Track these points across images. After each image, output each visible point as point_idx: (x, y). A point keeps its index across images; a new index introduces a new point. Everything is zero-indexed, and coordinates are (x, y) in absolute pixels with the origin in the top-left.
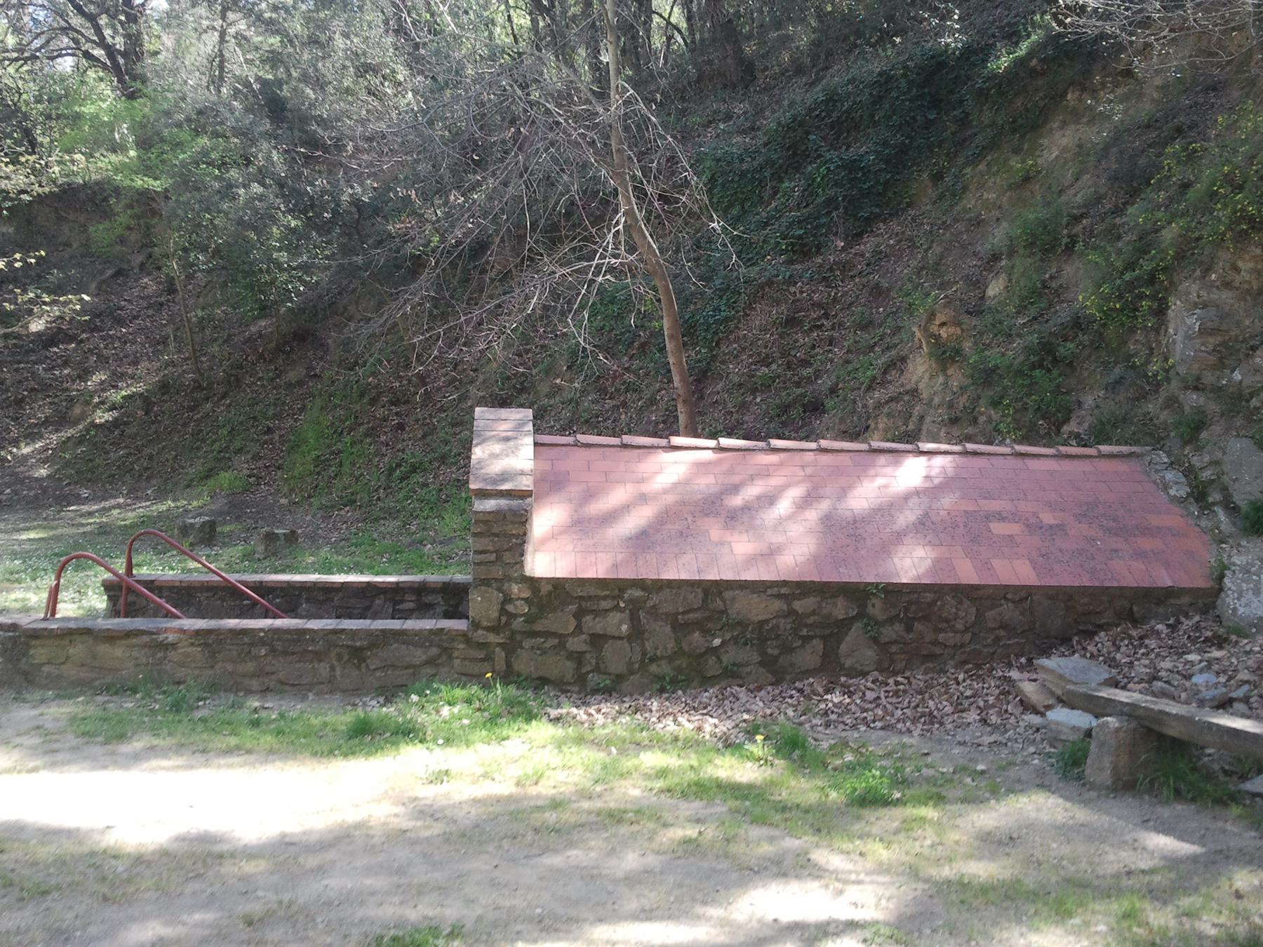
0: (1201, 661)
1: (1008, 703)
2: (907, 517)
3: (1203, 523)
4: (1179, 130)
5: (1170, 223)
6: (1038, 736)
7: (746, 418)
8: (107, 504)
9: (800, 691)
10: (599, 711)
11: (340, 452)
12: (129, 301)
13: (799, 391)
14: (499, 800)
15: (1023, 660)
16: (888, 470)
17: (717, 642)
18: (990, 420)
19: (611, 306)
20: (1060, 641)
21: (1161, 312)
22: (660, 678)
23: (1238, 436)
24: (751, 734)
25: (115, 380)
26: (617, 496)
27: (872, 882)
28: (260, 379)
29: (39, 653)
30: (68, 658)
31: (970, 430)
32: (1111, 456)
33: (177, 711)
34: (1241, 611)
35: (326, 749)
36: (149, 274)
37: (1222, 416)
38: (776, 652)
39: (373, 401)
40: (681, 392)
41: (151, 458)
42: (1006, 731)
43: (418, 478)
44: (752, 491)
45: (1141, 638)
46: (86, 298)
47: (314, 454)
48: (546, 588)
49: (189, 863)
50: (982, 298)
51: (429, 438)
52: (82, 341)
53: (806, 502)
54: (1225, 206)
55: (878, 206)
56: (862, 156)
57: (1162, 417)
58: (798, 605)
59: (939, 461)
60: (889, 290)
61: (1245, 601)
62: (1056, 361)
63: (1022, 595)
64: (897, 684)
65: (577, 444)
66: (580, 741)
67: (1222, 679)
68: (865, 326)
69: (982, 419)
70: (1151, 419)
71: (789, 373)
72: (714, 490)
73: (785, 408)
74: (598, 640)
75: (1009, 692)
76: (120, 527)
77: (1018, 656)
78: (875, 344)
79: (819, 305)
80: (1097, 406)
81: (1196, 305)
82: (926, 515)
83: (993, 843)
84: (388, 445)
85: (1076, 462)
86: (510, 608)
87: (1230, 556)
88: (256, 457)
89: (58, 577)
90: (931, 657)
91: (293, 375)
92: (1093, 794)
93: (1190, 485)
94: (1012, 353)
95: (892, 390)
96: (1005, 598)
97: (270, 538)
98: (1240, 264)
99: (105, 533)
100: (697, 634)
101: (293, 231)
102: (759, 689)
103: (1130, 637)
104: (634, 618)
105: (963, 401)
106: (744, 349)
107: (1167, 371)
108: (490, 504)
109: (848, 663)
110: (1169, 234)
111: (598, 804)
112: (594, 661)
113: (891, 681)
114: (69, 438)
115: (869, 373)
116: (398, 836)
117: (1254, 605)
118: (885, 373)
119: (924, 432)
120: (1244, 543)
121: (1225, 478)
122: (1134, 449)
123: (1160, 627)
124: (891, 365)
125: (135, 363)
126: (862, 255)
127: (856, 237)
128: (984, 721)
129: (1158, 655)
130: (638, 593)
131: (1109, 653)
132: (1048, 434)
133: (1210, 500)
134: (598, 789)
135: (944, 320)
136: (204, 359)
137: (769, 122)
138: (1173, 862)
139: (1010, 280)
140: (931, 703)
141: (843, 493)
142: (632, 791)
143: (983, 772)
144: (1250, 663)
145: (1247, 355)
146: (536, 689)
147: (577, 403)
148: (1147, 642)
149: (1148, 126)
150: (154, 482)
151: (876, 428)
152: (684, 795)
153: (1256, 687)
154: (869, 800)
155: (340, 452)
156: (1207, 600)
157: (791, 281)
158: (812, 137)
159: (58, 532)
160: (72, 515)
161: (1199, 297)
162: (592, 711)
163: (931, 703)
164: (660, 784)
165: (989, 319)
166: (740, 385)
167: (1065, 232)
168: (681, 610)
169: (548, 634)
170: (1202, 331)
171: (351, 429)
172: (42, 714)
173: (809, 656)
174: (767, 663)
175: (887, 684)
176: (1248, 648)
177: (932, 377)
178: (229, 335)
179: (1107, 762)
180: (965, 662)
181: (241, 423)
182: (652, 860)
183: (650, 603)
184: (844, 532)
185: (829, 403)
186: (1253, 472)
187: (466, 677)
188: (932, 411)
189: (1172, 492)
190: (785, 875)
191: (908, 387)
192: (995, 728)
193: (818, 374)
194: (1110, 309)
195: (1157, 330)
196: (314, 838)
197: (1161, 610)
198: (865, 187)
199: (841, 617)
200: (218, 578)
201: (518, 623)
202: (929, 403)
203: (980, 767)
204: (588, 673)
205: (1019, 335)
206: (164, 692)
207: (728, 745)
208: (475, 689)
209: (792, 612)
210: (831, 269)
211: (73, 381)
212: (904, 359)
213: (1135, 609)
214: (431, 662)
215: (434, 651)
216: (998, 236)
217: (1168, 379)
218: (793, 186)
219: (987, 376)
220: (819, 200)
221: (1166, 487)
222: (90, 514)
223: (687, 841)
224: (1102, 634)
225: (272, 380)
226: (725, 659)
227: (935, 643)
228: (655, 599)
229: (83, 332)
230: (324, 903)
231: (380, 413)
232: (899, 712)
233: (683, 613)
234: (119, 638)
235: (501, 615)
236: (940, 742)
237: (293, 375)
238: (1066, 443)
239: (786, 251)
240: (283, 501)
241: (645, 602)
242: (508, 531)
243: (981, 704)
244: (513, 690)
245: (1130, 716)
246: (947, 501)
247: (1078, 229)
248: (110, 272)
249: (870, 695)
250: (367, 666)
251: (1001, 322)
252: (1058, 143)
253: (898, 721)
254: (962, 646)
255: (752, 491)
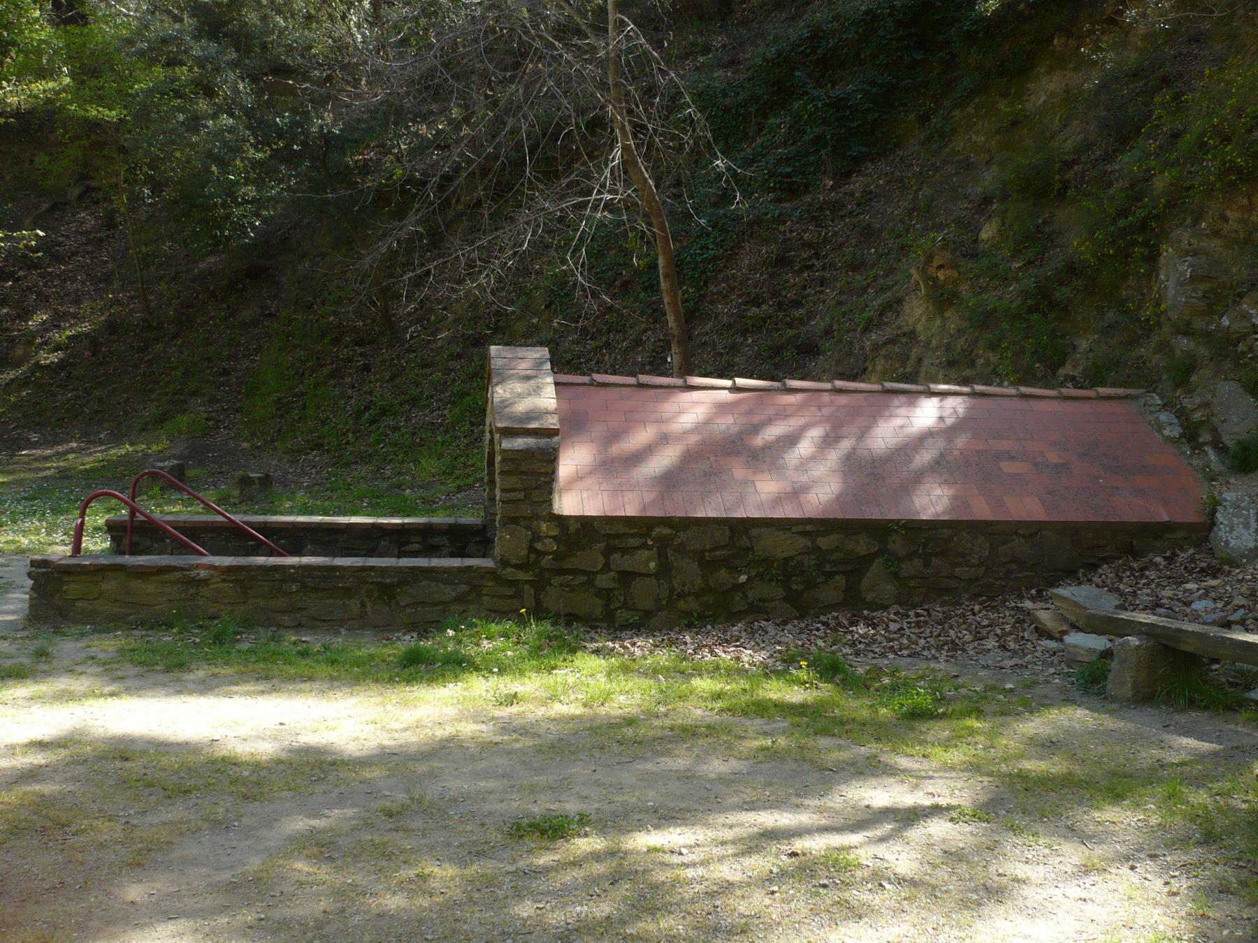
0: (1198, 589)
1: (1024, 630)
2: (925, 457)
3: (1195, 462)
4: (1166, 81)
5: (1162, 172)
6: (1055, 659)
7: (737, 360)
8: (60, 449)
9: (825, 624)
10: (634, 644)
11: (303, 394)
12: (67, 237)
13: (791, 332)
14: (573, 718)
15: (1033, 592)
16: (903, 411)
17: (743, 578)
18: (988, 363)
19: (607, 243)
20: (1070, 574)
21: (1152, 258)
22: (687, 614)
23: (1226, 379)
24: (790, 661)
25: (56, 323)
26: (641, 437)
27: (941, 778)
28: (212, 318)
29: (72, 588)
30: (101, 593)
31: (968, 373)
32: (1108, 398)
33: (221, 644)
34: (1233, 543)
35: (386, 677)
36: (86, 208)
37: (1212, 359)
38: (800, 587)
39: (336, 341)
40: (676, 332)
41: (101, 401)
42: (1025, 655)
43: (389, 421)
44: (774, 431)
45: (1142, 569)
46: (41, 234)
47: (276, 396)
48: (573, 527)
49: (307, 769)
50: (976, 241)
51: (397, 381)
52: (18, 279)
53: (828, 442)
54: (1215, 156)
55: (866, 145)
56: (849, 94)
57: (1154, 361)
58: (823, 542)
59: (951, 402)
60: (880, 231)
61: (1236, 535)
62: (1052, 305)
63: (1032, 530)
64: (917, 615)
65: (593, 384)
66: (626, 669)
67: (1220, 605)
68: (855, 268)
69: (981, 361)
70: (1144, 363)
71: (781, 315)
72: (735, 430)
73: (777, 350)
74: (626, 577)
75: (1023, 621)
76: (81, 472)
77: (1028, 588)
78: (868, 285)
79: (810, 245)
80: (1091, 350)
81: (1187, 253)
82: (942, 455)
83: (1048, 746)
84: (353, 387)
85: (1077, 404)
86: (539, 546)
87: (1221, 493)
88: (213, 400)
89: (83, 515)
90: (948, 590)
91: (247, 314)
92: (1115, 706)
93: (1182, 426)
94: (1009, 296)
95: (889, 332)
96: (1016, 533)
97: (245, 481)
98: (1228, 213)
99: (66, 477)
100: (723, 572)
101: (260, 163)
102: (785, 623)
103: (1131, 569)
104: (662, 555)
105: (961, 343)
106: (732, 289)
107: (1158, 316)
108: (520, 443)
109: (869, 597)
110: (1160, 183)
111: (668, 722)
112: (622, 598)
113: (912, 613)
114: (12, 380)
115: (866, 315)
116: (488, 748)
117: (1244, 538)
118: (881, 315)
119: (922, 375)
120: (1232, 480)
121: (1215, 420)
122: (1131, 391)
123: (1158, 559)
124: (887, 307)
125: (77, 302)
126: (852, 195)
127: (844, 176)
128: (1004, 647)
129: (1158, 585)
130: (666, 531)
131: (1113, 584)
132: (1044, 377)
133: (1201, 440)
134: (662, 709)
135: (941, 262)
136: (151, 297)
137: (755, 54)
138: (1201, 757)
139: (1003, 224)
140: (952, 632)
141: (863, 434)
142: (697, 712)
143: (1011, 690)
144: (1244, 590)
145: (1235, 302)
146: (568, 624)
147: (557, 344)
148: (1147, 573)
149: (1135, 75)
150: (106, 425)
151: (874, 370)
152: (745, 713)
153: (1250, 611)
154: (916, 715)
155: (303, 394)
156: (1201, 533)
157: (781, 220)
158: (797, 73)
159: (17, 477)
160: (26, 459)
161: (1189, 244)
162: (627, 644)
163: (952, 632)
164: (719, 705)
165: (985, 262)
166: (730, 326)
167: (1057, 177)
168: (708, 547)
169: (576, 572)
170: (1194, 279)
171: (313, 370)
172: (88, 647)
173: (831, 592)
174: (792, 598)
175: (908, 616)
176: (1240, 577)
177: (929, 319)
178: (177, 273)
179: (1128, 678)
180: (980, 595)
181: (195, 364)
182: (734, 764)
183: (678, 541)
184: (866, 471)
185: (826, 344)
186: (1239, 414)
187: (500, 614)
188: (930, 354)
189: (1166, 432)
190: (861, 773)
191: (905, 329)
192: (1015, 652)
193: (811, 315)
194: (1103, 255)
195: (1148, 276)
196: (413, 749)
197: (1158, 544)
198: (854, 125)
199: (863, 553)
200: (220, 518)
201: (547, 561)
202: (927, 345)
203: (1009, 686)
204: (617, 609)
205: (1017, 280)
206: (200, 627)
207: (768, 672)
208: (509, 625)
209: (816, 549)
210: (821, 209)
211: (13, 320)
212: (900, 301)
213: (1135, 543)
214: (460, 599)
215: (463, 588)
216: (989, 179)
217: (1159, 324)
218: (779, 123)
219: (984, 320)
220: (806, 138)
221: (1160, 428)
222: (46, 458)
223: (764, 749)
224: (1105, 566)
225: (226, 319)
226: (750, 594)
227: (952, 577)
228: (683, 536)
229: (20, 269)
230: (449, 800)
231: (345, 353)
232: (922, 642)
233: (710, 550)
234: (152, 574)
235: (529, 552)
236: (965, 666)
237: (247, 314)
238: (1062, 385)
239: (774, 189)
240: (245, 445)
241: (672, 539)
242: (537, 470)
243: (999, 632)
244: (547, 626)
245: (1147, 634)
246: (961, 441)
247: (1070, 175)
248: (45, 206)
249: (893, 627)
250: (397, 603)
251: (997, 265)
252: (1045, 88)
253: (923, 649)
254: (976, 579)
255: (774, 431)
